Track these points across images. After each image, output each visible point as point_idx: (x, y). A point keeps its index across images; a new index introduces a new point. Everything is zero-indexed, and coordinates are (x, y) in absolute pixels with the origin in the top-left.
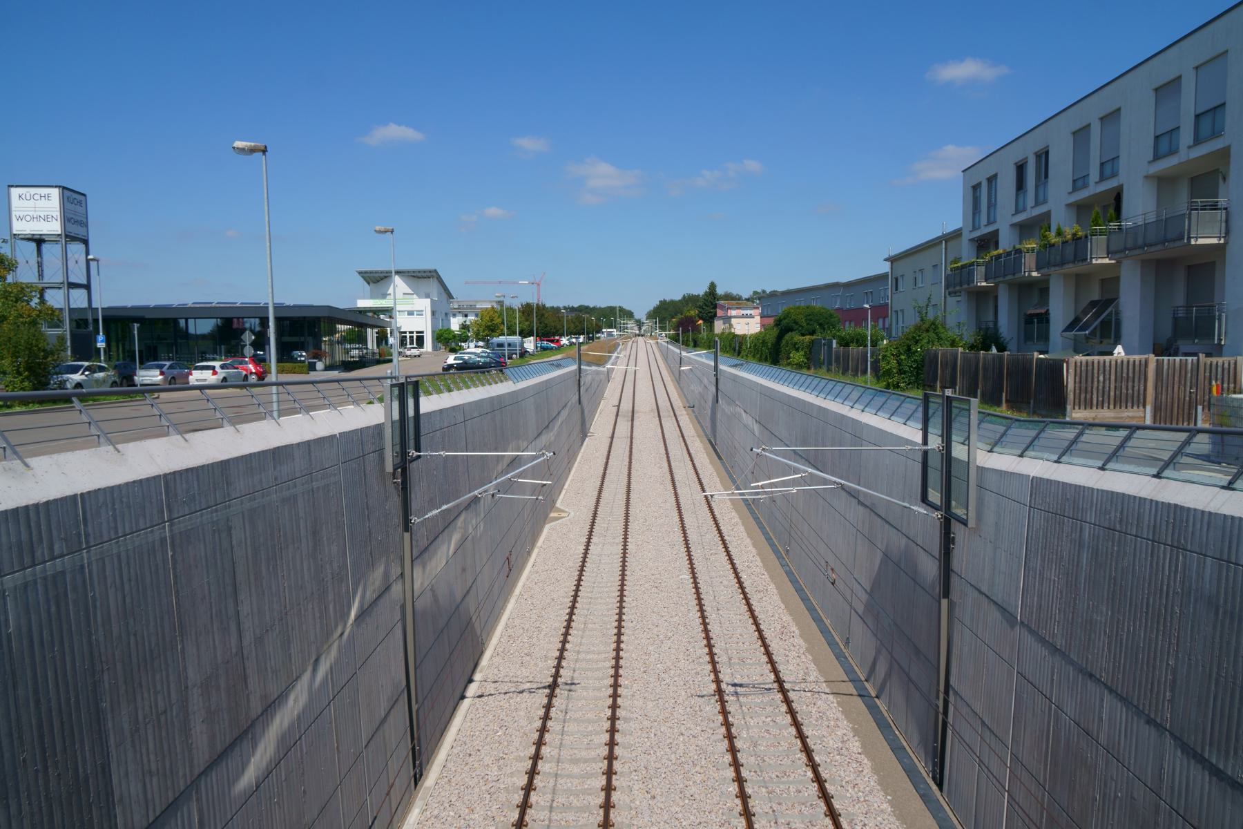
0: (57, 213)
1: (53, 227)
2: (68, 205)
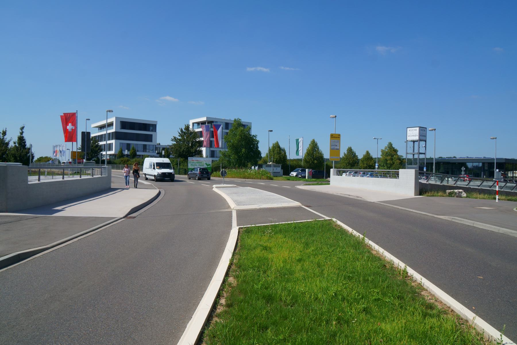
0: (418, 134)
1: (417, 138)
2: (421, 132)
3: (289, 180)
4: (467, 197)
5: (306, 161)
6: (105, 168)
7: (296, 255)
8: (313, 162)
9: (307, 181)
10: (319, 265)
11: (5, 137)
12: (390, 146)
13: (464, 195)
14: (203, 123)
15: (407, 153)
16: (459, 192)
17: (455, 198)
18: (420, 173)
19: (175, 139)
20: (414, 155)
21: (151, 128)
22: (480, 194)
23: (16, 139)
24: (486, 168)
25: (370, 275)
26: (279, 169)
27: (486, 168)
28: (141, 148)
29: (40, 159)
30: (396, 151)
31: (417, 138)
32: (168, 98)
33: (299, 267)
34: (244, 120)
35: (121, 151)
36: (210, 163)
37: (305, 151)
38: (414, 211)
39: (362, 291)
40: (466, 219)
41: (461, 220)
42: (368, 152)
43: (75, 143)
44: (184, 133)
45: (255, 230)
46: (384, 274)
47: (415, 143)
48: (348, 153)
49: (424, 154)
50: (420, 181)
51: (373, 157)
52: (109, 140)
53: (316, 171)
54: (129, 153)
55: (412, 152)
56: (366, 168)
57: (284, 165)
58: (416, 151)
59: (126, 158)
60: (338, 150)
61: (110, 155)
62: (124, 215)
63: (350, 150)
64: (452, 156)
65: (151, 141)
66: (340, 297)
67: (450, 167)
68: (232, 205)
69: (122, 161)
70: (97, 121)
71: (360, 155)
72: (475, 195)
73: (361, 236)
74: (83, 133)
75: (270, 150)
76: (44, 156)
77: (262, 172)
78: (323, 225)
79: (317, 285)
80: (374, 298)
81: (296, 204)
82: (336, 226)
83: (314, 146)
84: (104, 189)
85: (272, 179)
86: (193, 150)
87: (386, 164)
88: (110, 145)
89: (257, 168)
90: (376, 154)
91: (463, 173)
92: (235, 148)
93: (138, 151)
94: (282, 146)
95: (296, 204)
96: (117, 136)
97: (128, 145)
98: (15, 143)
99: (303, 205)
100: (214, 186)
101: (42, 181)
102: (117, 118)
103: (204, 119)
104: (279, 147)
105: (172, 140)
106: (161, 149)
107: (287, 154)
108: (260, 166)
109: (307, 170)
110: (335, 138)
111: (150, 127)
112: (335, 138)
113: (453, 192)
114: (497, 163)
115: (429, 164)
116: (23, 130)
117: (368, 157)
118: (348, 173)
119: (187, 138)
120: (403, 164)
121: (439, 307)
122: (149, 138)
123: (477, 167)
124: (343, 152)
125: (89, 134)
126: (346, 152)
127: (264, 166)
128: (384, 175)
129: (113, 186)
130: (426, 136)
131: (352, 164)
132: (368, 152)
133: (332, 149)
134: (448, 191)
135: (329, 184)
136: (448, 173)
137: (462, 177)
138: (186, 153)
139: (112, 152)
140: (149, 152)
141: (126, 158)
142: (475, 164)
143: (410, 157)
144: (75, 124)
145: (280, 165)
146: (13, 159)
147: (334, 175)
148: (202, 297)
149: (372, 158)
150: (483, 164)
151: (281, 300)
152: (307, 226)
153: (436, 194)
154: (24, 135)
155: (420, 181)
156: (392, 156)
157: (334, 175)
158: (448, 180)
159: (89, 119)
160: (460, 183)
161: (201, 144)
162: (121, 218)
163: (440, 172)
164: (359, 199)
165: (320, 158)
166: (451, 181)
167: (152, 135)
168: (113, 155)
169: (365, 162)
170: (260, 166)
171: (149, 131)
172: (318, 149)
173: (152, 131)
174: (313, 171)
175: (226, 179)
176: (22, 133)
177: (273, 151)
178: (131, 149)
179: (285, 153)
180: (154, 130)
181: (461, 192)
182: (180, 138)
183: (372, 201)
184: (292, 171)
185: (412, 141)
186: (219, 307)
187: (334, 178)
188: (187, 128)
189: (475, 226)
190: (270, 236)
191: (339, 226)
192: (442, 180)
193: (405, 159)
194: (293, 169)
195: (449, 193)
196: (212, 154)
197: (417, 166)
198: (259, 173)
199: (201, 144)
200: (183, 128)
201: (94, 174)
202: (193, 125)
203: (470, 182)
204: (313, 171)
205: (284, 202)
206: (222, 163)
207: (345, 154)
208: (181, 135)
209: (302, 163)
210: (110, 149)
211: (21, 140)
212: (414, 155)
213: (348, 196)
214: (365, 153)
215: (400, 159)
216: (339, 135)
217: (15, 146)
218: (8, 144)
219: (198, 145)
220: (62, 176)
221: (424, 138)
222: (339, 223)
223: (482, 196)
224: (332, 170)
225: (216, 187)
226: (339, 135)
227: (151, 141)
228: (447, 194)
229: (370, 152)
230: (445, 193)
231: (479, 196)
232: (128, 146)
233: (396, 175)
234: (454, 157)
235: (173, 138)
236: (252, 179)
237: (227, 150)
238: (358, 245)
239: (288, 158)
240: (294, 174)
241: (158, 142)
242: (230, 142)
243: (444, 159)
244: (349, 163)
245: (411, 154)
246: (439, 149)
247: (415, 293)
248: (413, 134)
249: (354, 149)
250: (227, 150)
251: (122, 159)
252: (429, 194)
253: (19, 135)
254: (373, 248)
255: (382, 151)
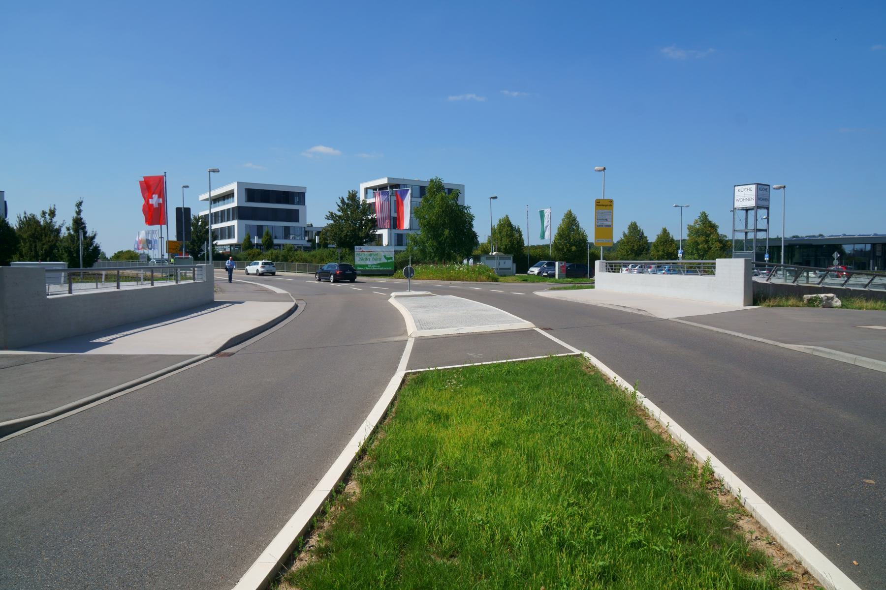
0: (754, 197)
1: (752, 203)
2: (760, 192)
3: (526, 281)
4: (842, 306)
5: (556, 246)
6: (201, 267)
7: (491, 434)
8: (569, 250)
9: (557, 282)
10: (531, 457)
11: (54, 220)
12: (704, 217)
13: (837, 302)
14: (382, 188)
15: (734, 231)
16: (828, 298)
17: (820, 308)
18: (756, 264)
19: (332, 216)
20: (746, 233)
21: (297, 199)
22: (867, 300)
23: (70, 223)
24: (878, 253)
25: (632, 479)
26: (509, 264)
27: (878, 253)
28: (281, 233)
29: (118, 256)
30: (714, 227)
31: (752, 203)
32: (321, 149)
33: (489, 462)
34: (449, 179)
35: (248, 239)
36: (392, 255)
37: (555, 231)
38: (740, 335)
39: (606, 519)
40: (841, 350)
41: (830, 353)
42: (665, 231)
43: (164, 227)
44: (347, 204)
45: (443, 376)
46: (662, 477)
47: (749, 212)
48: (630, 232)
49: (765, 230)
50: (754, 279)
51: (675, 239)
52: (228, 220)
53: (573, 265)
54: (260, 242)
55: (743, 228)
56: (661, 258)
57: (518, 255)
58: (751, 226)
59: (256, 250)
60: (610, 227)
61: (231, 245)
62: (214, 350)
63: (634, 228)
64: (817, 234)
65: (297, 220)
66: (555, 539)
67: (812, 253)
68: (412, 329)
69: (249, 255)
70: (204, 189)
71: (652, 236)
72: (858, 303)
73: (631, 389)
74: (178, 210)
75: (493, 230)
76: (125, 250)
77: (480, 268)
78: (562, 367)
79: (516, 509)
80: (629, 540)
81: (525, 324)
82: (588, 367)
83: (571, 222)
84: (203, 302)
85: (496, 280)
86: (362, 234)
87: (697, 250)
88: (230, 229)
89: (471, 261)
90: (679, 234)
91: (836, 262)
92: (433, 229)
93: (276, 238)
94: (514, 223)
95: (525, 324)
96: (241, 213)
97: (260, 228)
98: (68, 229)
99: (537, 326)
100: (393, 294)
101: (75, 293)
102: (239, 184)
103: (384, 181)
104: (510, 225)
105: (327, 218)
106: (314, 233)
107: (524, 237)
108: (477, 259)
109: (557, 263)
110: (604, 206)
111: (294, 197)
112: (604, 206)
113: (817, 298)
114: (785, 246)
115: (774, 248)
116: (81, 208)
117: (665, 239)
118: (630, 267)
119: (352, 213)
120: (726, 249)
121: (777, 561)
122: (294, 216)
123: (862, 253)
124: (619, 233)
125: (188, 210)
126: (626, 232)
127: (483, 258)
128: (692, 270)
129: (217, 297)
130: (768, 200)
131: (638, 251)
132: (665, 231)
133: (598, 227)
134: (807, 297)
135: (593, 287)
136: (808, 263)
137: (834, 271)
138: (350, 238)
139: (234, 241)
140: (294, 238)
141: (256, 250)
142: (858, 247)
143: (741, 236)
144: (162, 194)
145: (511, 256)
146: (66, 255)
147: (601, 271)
148: (282, 527)
149: (672, 240)
150: (874, 245)
151: (431, 542)
152: (532, 369)
153: (784, 301)
154: (82, 215)
155: (754, 279)
156: (708, 236)
157: (601, 271)
158: (808, 277)
159: (187, 187)
160: (829, 282)
161: (374, 224)
162: (208, 357)
163: (791, 263)
164: (640, 313)
165: (582, 242)
166: (813, 278)
167: (298, 211)
168: (236, 245)
169: (661, 248)
170: (477, 259)
171: (293, 203)
172: (578, 226)
173: (298, 204)
174: (567, 265)
175: (413, 282)
176: (79, 213)
177: (500, 233)
178: (264, 234)
179: (521, 235)
180: (302, 201)
181: (832, 298)
182: (340, 213)
183: (665, 317)
184: (532, 266)
185: (743, 209)
186: (303, 555)
187: (601, 276)
188: (353, 196)
189: (857, 364)
190: (455, 391)
191: (594, 368)
192: (797, 276)
193: (731, 241)
194: (534, 262)
195: (809, 300)
196: (399, 239)
197: (752, 253)
198: (473, 270)
199: (374, 224)
200: (346, 196)
201: (192, 276)
202: (366, 193)
203: (849, 278)
204: (567, 265)
205: (503, 322)
206: (413, 255)
207: (625, 235)
208: (341, 209)
209: (551, 252)
210: (230, 236)
211: (79, 224)
212: (746, 233)
213: (622, 309)
214: (659, 232)
215: (721, 241)
216: (611, 201)
217: (69, 234)
218: (58, 231)
219: (370, 225)
220: (115, 284)
221: (765, 203)
222: (594, 361)
223: (870, 304)
224: (597, 263)
225: (396, 297)
226: (611, 201)
227: (297, 220)
228: (805, 301)
229: (669, 230)
230: (801, 299)
231: (864, 304)
232: (260, 231)
233: (710, 270)
234: (821, 235)
235: (328, 214)
236: (463, 280)
237: (419, 232)
238: (623, 410)
239: (526, 244)
240: (535, 270)
241: (308, 222)
242: (425, 218)
243: (802, 239)
244: (632, 250)
245: (741, 231)
246: (790, 223)
247: (723, 525)
248: (746, 196)
249: (641, 226)
250: (419, 232)
251: (249, 251)
252: (771, 303)
253: (75, 215)
254: (650, 414)
255: (690, 228)
